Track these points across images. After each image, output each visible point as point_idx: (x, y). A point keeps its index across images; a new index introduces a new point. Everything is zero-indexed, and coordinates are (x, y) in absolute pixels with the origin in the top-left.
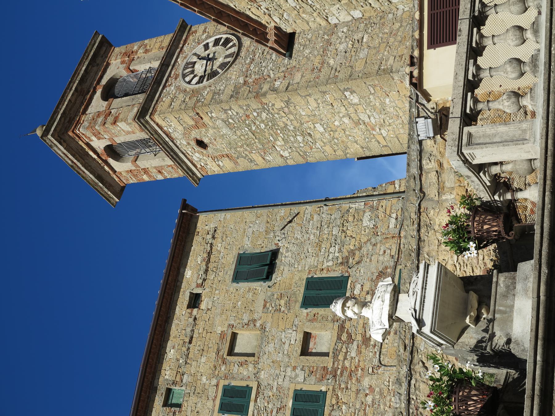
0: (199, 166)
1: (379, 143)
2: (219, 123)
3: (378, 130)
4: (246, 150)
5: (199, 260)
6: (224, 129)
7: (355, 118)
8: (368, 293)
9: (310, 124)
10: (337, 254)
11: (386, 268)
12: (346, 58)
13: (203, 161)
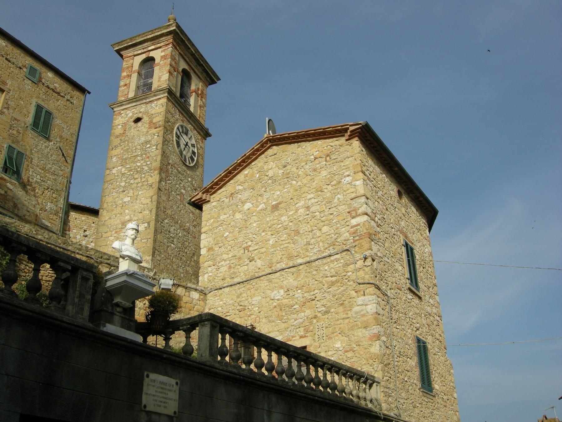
0: (122, 112)
3: (115, 235)
4: (125, 147)
6: (144, 139)
8: (6, 192)
10: (35, 179)
11: (18, 210)
12: (166, 231)
13: (125, 116)
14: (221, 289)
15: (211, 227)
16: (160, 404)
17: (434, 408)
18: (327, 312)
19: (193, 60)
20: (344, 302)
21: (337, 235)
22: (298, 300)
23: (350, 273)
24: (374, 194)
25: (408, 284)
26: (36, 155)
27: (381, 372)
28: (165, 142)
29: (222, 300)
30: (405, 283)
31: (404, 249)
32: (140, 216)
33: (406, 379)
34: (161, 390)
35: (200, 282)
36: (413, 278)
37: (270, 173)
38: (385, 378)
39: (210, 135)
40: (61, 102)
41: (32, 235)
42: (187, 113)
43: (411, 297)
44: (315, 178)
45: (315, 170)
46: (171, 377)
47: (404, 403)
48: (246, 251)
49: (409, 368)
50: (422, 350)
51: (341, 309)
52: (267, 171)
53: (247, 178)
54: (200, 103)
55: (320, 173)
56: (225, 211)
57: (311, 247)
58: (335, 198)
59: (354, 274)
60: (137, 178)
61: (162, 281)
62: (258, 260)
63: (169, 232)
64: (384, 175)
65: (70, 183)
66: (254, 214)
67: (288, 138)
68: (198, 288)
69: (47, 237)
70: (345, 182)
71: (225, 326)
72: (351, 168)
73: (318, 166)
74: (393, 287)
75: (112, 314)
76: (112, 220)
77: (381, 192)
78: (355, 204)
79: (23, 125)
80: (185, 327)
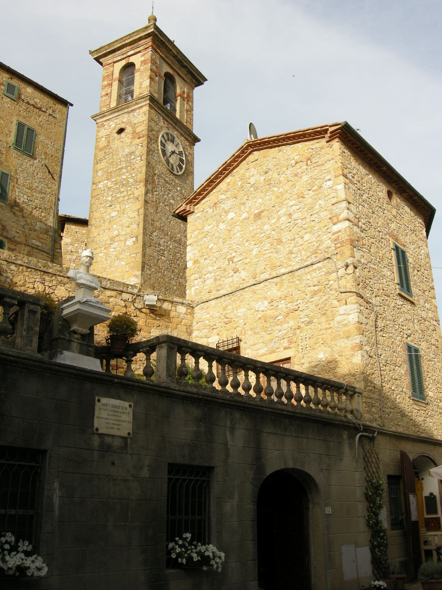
0: (105, 123)
1: (95, 249)
2: (133, 149)
3: (105, 251)
5: (37, 100)
7: (117, 239)
9: (118, 208)
10: (22, 199)
11: (7, 232)
14: (207, 301)
15: (196, 239)
16: (112, 426)
17: (427, 416)
18: (310, 322)
19: (177, 62)
20: (327, 312)
21: (319, 243)
22: (282, 311)
23: (332, 282)
24: (357, 198)
25: (398, 290)
26: (21, 175)
27: (363, 382)
28: (150, 152)
29: (209, 313)
30: (394, 288)
31: (393, 253)
32: (128, 230)
33: (393, 388)
34: (114, 413)
35: (187, 295)
36: (405, 282)
37: (252, 181)
38: (367, 389)
39: (198, 140)
40: (43, 118)
41: (11, 261)
42: (172, 120)
43: (402, 303)
44: (297, 184)
45: (296, 175)
46: (124, 400)
47: (390, 412)
48: (231, 262)
49: (397, 377)
50: (414, 358)
51: (324, 319)
52: (249, 179)
53: (229, 187)
54: (186, 106)
55: (301, 178)
56: (209, 222)
57: (294, 256)
58: (316, 204)
59: (336, 282)
60: (123, 192)
61: (146, 297)
62: (243, 271)
63: (159, 244)
64: (371, 176)
65: (59, 199)
66: (237, 224)
67: (269, 142)
68: (184, 302)
69: (26, 261)
70: (326, 187)
71: (184, 347)
72: (332, 172)
73: (299, 170)
74: (379, 294)
75: (70, 341)
76: (101, 236)
77: (367, 195)
78: (336, 209)
79: (5, 145)
80: (145, 349)
